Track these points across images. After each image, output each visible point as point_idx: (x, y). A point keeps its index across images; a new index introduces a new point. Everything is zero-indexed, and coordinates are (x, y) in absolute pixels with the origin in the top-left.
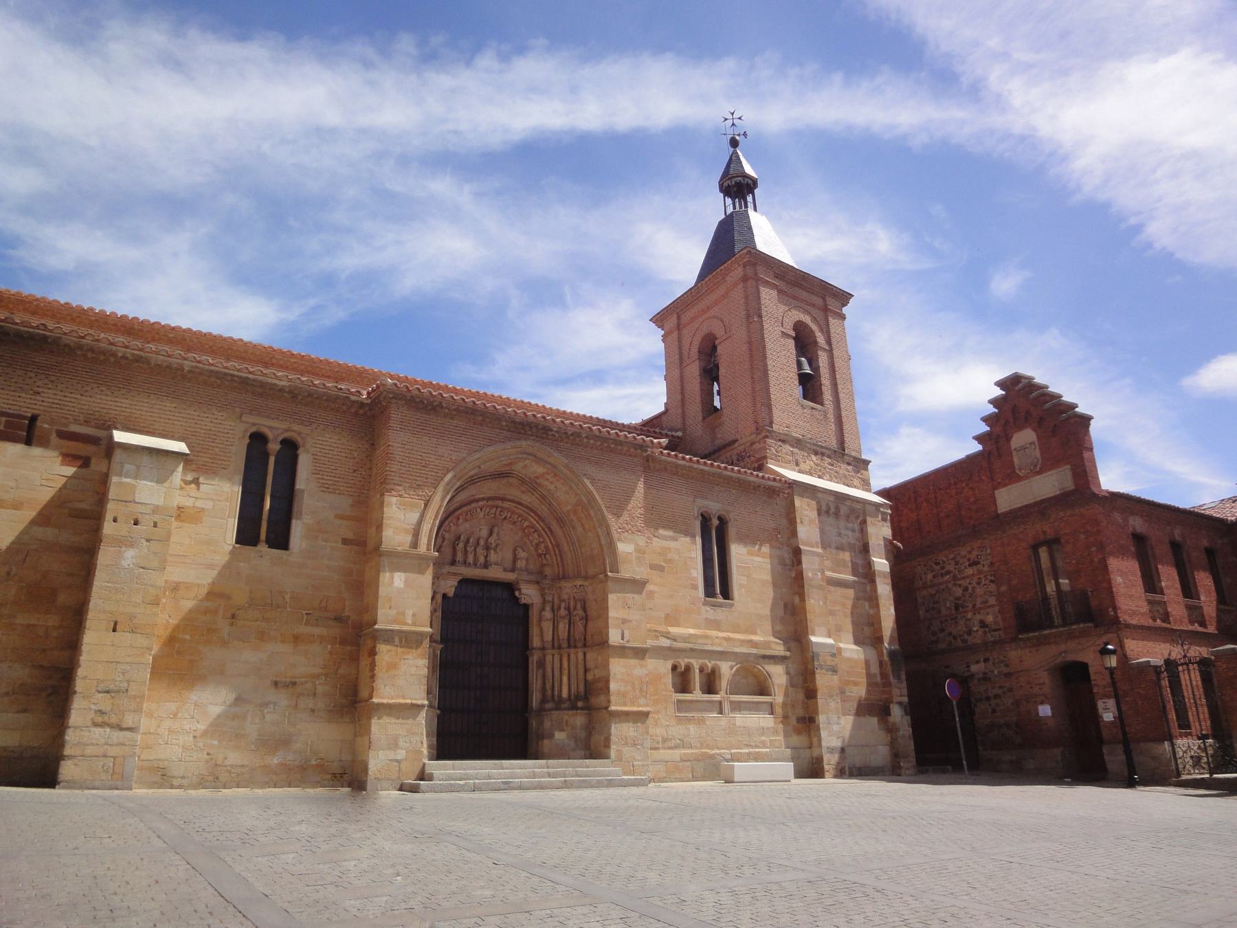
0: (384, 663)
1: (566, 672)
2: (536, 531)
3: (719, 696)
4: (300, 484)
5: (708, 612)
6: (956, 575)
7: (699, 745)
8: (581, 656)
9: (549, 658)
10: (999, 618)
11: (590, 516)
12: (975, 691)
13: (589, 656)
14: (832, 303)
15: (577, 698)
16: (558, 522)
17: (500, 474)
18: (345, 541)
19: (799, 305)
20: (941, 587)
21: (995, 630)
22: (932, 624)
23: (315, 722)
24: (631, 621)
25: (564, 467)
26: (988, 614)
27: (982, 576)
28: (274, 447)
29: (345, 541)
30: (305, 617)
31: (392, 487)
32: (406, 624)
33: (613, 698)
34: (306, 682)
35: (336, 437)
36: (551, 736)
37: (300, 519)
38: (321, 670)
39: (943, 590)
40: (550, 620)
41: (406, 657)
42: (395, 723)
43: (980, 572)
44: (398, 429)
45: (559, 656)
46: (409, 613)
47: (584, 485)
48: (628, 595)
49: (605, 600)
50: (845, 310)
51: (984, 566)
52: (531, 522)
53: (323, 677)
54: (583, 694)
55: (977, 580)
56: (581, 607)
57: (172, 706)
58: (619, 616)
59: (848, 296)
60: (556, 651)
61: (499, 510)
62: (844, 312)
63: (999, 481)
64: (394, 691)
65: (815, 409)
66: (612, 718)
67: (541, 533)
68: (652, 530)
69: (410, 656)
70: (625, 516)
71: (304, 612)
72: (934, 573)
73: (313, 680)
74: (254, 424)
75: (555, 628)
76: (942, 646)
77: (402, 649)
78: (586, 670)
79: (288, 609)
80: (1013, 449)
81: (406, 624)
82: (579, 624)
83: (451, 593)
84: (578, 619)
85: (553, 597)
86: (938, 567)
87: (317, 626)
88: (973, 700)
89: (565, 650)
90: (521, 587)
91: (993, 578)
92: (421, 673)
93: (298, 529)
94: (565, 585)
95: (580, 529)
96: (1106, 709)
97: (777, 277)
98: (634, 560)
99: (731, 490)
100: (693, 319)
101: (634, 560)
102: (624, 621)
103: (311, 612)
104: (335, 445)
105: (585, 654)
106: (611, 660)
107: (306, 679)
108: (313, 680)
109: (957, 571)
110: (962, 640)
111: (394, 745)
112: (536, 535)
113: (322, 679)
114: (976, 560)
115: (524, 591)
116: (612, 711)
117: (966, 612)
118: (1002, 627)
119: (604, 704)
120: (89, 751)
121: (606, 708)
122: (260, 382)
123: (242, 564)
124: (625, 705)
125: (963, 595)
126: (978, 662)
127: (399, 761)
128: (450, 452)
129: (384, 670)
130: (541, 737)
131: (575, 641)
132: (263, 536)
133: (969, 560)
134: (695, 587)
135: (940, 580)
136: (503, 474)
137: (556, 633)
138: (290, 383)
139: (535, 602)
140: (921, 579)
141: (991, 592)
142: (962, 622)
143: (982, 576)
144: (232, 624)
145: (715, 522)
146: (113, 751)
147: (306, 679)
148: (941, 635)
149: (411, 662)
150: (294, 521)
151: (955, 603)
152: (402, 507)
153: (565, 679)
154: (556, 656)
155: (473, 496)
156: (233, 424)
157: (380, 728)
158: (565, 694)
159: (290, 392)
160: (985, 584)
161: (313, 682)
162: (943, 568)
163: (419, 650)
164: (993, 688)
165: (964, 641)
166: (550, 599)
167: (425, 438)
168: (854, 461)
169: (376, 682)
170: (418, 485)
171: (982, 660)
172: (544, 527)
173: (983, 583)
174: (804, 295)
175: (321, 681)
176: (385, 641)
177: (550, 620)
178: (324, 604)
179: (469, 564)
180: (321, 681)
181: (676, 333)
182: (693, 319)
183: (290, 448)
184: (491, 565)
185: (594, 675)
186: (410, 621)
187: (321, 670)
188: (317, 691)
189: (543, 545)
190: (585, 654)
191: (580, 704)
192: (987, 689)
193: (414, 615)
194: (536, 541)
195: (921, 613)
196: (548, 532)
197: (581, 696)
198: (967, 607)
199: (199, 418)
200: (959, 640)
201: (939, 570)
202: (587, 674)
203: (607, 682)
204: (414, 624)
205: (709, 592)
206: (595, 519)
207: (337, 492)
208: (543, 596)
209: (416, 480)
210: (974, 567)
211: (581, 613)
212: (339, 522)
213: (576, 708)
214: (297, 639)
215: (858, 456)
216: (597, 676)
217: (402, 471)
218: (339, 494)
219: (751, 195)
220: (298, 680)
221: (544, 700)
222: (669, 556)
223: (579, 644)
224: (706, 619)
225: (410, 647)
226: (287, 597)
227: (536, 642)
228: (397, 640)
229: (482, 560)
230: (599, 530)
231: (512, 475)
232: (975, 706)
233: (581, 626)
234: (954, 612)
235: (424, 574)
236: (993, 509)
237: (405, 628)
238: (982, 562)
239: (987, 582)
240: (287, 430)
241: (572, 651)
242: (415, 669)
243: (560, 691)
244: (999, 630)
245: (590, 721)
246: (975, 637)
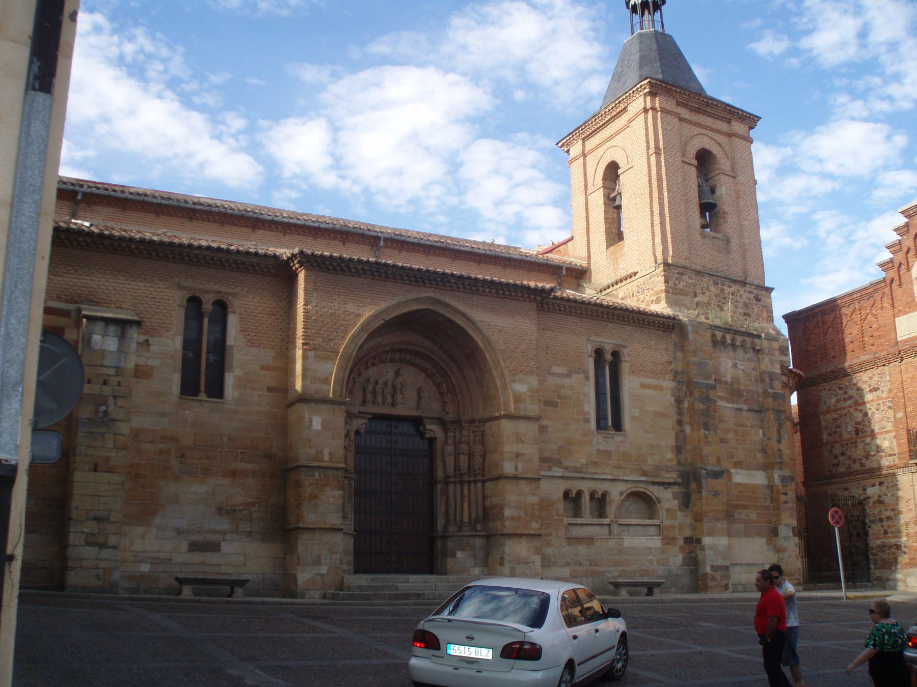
1: (466, 499)
3: (608, 520)
5: (599, 442)
6: (858, 401)
7: (588, 563)
10: (895, 443)
12: (870, 513)
14: (738, 127)
18: (270, 389)
19: (700, 132)
20: (844, 412)
21: (890, 455)
22: (834, 447)
26: (885, 439)
27: (880, 402)
28: (208, 307)
29: (270, 389)
34: (244, 510)
37: (231, 371)
39: (845, 415)
43: (879, 398)
46: (326, 451)
50: (752, 133)
51: (883, 392)
53: (257, 505)
55: (876, 406)
57: (141, 529)
59: (755, 119)
62: (751, 135)
63: (900, 308)
65: (715, 238)
71: (239, 451)
72: (837, 398)
75: (457, 460)
76: (841, 469)
79: (226, 449)
80: (913, 277)
81: (323, 461)
86: (841, 392)
88: (867, 521)
91: (891, 405)
93: (230, 380)
96: (875, 543)
97: (680, 106)
99: (625, 326)
100: (597, 147)
102: (518, 455)
103: (244, 451)
104: (259, 304)
107: (243, 507)
109: (858, 396)
110: (860, 464)
111: (318, 562)
114: (876, 386)
117: (865, 437)
118: (896, 452)
120: (85, 563)
123: (186, 412)
125: (863, 420)
126: (873, 485)
127: (323, 575)
130: (445, 555)
132: (203, 388)
133: (870, 385)
134: (587, 421)
135: (843, 404)
140: (826, 403)
141: (888, 418)
142: (860, 446)
143: (880, 402)
144: (182, 462)
145: (609, 357)
146: (102, 564)
147: (243, 507)
148: (841, 458)
150: (227, 374)
151: (856, 428)
153: (466, 505)
156: (173, 291)
157: (306, 545)
160: (883, 411)
162: (845, 393)
164: (886, 510)
165: (862, 465)
168: (755, 289)
171: (877, 483)
173: (882, 409)
174: (708, 121)
175: (255, 509)
179: (378, 404)
180: (255, 509)
181: (581, 159)
182: (597, 147)
183: (222, 307)
184: (397, 404)
186: (326, 457)
192: (881, 512)
193: (330, 454)
195: (825, 436)
198: (866, 432)
199: (137, 287)
200: (858, 464)
201: (841, 395)
204: (331, 461)
205: (601, 425)
207: (262, 346)
210: (874, 393)
212: (263, 372)
214: (234, 473)
215: (761, 285)
218: (264, 348)
219: (659, 11)
220: (236, 508)
222: (563, 392)
224: (598, 450)
226: (225, 439)
232: (870, 527)
234: (854, 436)
236: (893, 336)
238: (881, 389)
239: (885, 407)
243: (462, 515)
244: (895, 455)
246: (872, 461)
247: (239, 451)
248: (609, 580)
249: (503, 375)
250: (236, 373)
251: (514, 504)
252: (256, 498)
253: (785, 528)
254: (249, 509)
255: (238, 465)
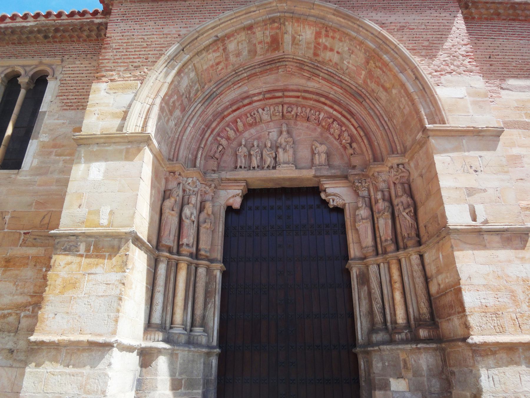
0: (59, 281)
1: (398, 285)
2: (334, 120)
4: (44, 107)
8: (415, 259)
9: (373, 269)
11: (386, 64)
13: (426, 256)
15: (420, 323)
16: (355, 98)
17: (271, 61)
23: (11, 367)
24: (485, 191)
25: (334, 15)
30: (22, 237)
31: (104, 73)
32: (99, 225)
33: (473, 320)
34: (10, 314)
35: (87, 62)
36: (386, 386)
37: (37, 138)
38: (30, 299)
40: (367, 219)
41: (93, 271)
42: (61, 374)
44: (119, 21)
45: (386, 265)
47: (367, 29)
48: (472, 153)
49: (432, 165)
52: (326, 112)
53: (31, 308)
54: (427, 316)
56: (405, 191)
58: (458, 185)
60: (380, 259)
61: (285, 107)
64: (68, 322)
66: (479, 359)
67: (342, 121)
68: (498, 82)
69: (99, 270)
70: (442, 56)
71: (22, 232)
73: (18, 312)
74: (8, 67)
77: (89, 260)
78: (427, 280)
82: (404, 214)
83: (237, 203)
84: (401, 209)
85: (369, 191)
87: (34, 246)
89: (390, 255)
90: (325, 186)
92: (113, 293)
94: (377, 170)
95: (383, 95)
98: (469, 106)
101: (469, 106)
102: (471, 192)
103: (30, 231)
105: (421, 257)
106: (456, 254)
107: (10, 311)
108: (18, 312)
112: (335, 125)
113: (29, 310)
115: (329, 191)
116: (475, 344)
119: (460, 332)
121: (464, 339)
122: (11, 28)
124: (502, 330)
128: (179, 29)
129: (57, 291)
131: (403, 238)
136: (274, 60)
137: (378, 235)
138: (36, 23)
139: (346, 202)
147: (10, 311)
149: (99, 278)
152: (111, 92)
154: (382, 265)
155: (245, 92)
158: (401, 318)
159: (39, 31)
161: (17, 314)
163: (114, 260)
166: (366, 193)
167: (152, 23)
169: (42, 310)
170: (135, 67)
172: (340, 110)
175: (27, 313)
176: (65, 250)
177: (367, 219)
178: (46, 221)
180: (27, 313)
185: (439, 285)
186: (104, 221)
187: (30, 299)
188: (20, 326)
189: (346, 134)
190: (421, 257)
191: (423, 333)
193: (112, 213)
194: (337, 132)
196: (349, 117)
197: (425, 321)
202: (201, 214)
203: (458, 291)
206: (391, 64)
208: (356, 192)
209: (133, 62)
211: (405, 199)
213: (416, 339)
216: (442, 286)
217: (118, 57)
221: (373, 330)
223: (410, 243)
225: (103, 257)
226: (7, 217)
227: (354, 251)
228: (82, 248)
229: (269, 161)
230: (402, 77)
231: (286, 60)
233: (408, 217)
235: (132, 160)
237: (95, 230)
240: (37, 66)
241: (401, 254)
242: (104, 287)
243: (394, 314)
245: (444, 361)
247: (22, 232)
248: (213, 168)
249: (417, 78)
250: (41, 140)
251: (482, 282)
252: (32, 296)
253: (180, 339)
254: (17, 314)
255: (18, 251)
